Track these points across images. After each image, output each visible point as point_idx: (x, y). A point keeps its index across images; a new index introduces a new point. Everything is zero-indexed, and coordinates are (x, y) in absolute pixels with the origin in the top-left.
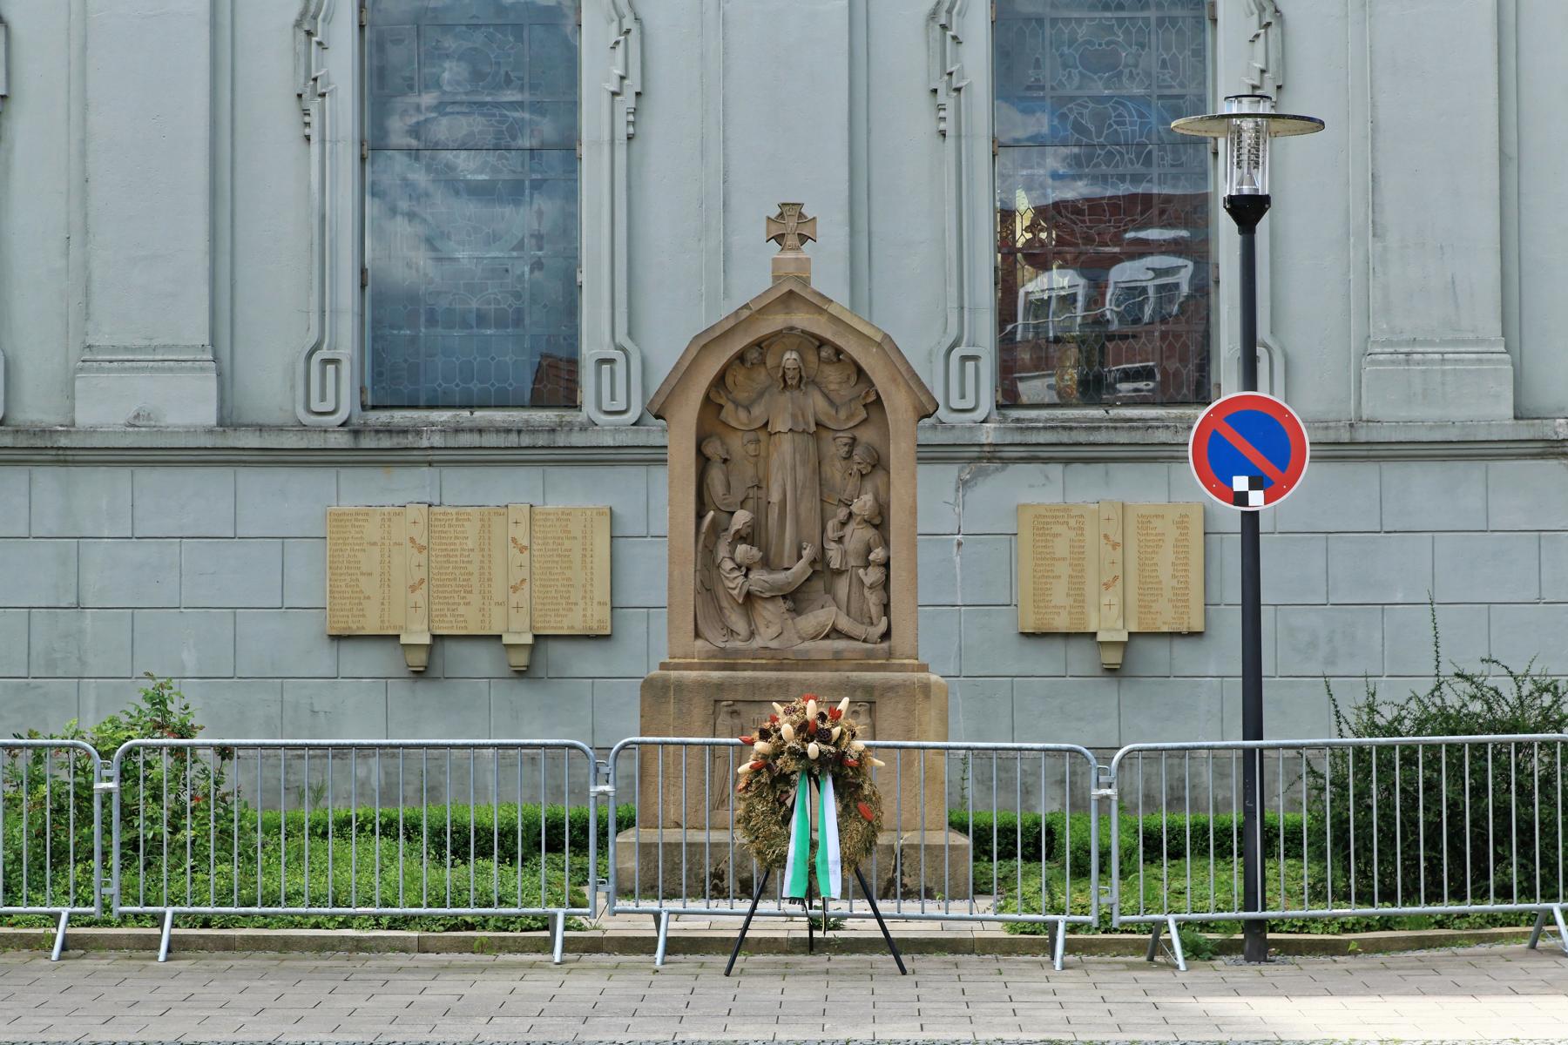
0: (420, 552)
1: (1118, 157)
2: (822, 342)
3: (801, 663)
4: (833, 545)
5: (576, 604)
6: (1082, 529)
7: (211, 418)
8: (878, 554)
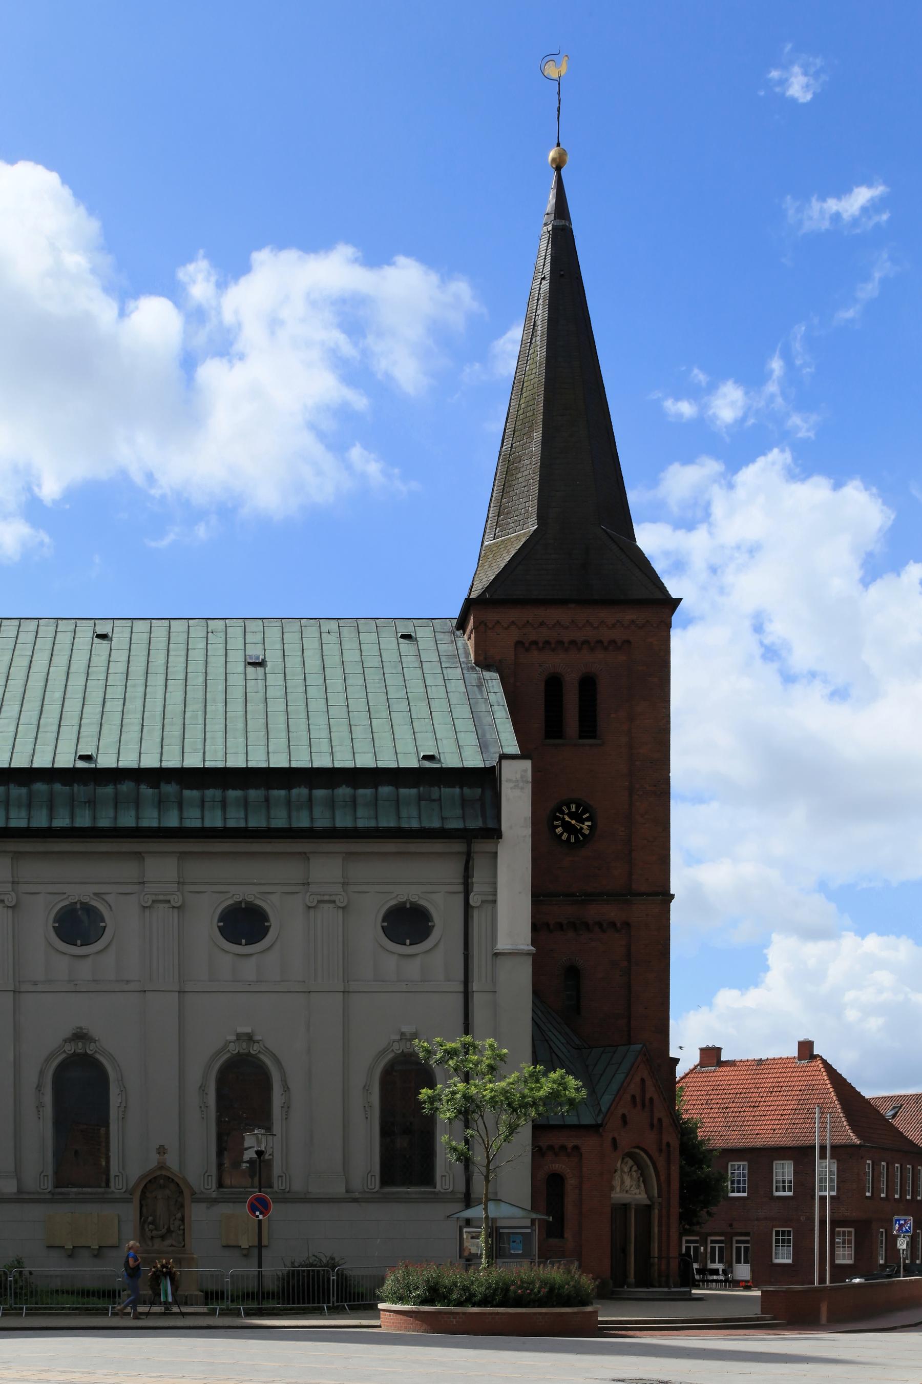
2: (169, 1178)
7: (15, 1190)
8: (182, 1227)
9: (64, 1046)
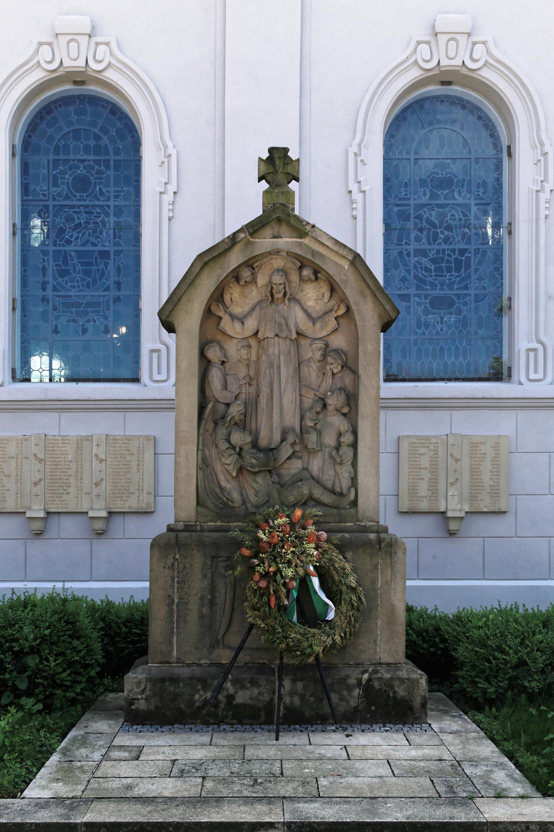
0: (40, 463)
5: (133, 493)
6: (437, 450)
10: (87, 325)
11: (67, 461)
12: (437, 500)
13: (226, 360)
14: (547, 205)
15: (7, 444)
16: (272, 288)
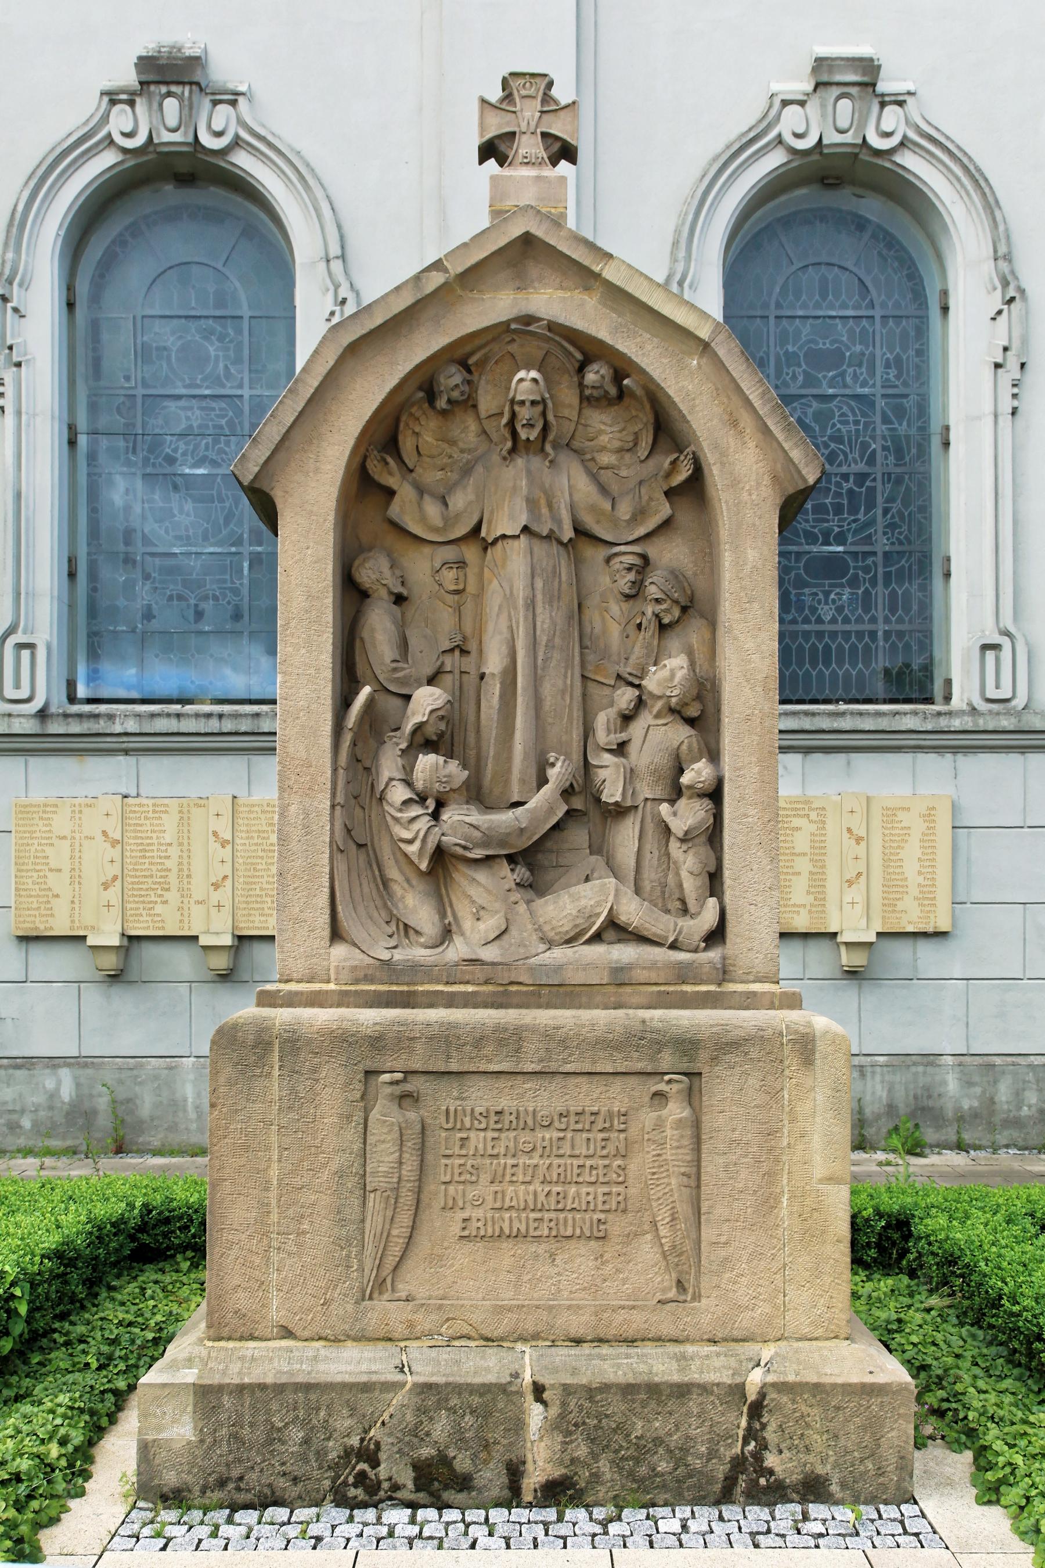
0: (113, 847)
1: (841, 457)
3: (545, 991)
4: (607, 758)
6: (824, 822)
8: (698, 773)
9: (105, 119)
10: (203, 605)
11: (162, 844)
12: (824, 912)
13: (405, 593)
14: (1016, 390)
15: (55, 812)
16: (513, 415)
